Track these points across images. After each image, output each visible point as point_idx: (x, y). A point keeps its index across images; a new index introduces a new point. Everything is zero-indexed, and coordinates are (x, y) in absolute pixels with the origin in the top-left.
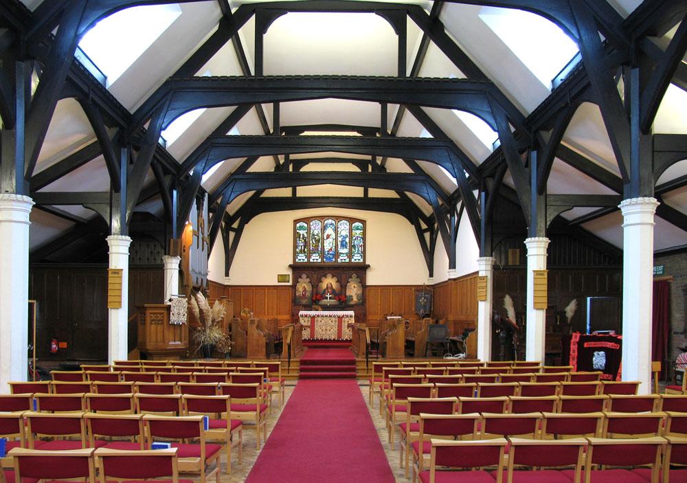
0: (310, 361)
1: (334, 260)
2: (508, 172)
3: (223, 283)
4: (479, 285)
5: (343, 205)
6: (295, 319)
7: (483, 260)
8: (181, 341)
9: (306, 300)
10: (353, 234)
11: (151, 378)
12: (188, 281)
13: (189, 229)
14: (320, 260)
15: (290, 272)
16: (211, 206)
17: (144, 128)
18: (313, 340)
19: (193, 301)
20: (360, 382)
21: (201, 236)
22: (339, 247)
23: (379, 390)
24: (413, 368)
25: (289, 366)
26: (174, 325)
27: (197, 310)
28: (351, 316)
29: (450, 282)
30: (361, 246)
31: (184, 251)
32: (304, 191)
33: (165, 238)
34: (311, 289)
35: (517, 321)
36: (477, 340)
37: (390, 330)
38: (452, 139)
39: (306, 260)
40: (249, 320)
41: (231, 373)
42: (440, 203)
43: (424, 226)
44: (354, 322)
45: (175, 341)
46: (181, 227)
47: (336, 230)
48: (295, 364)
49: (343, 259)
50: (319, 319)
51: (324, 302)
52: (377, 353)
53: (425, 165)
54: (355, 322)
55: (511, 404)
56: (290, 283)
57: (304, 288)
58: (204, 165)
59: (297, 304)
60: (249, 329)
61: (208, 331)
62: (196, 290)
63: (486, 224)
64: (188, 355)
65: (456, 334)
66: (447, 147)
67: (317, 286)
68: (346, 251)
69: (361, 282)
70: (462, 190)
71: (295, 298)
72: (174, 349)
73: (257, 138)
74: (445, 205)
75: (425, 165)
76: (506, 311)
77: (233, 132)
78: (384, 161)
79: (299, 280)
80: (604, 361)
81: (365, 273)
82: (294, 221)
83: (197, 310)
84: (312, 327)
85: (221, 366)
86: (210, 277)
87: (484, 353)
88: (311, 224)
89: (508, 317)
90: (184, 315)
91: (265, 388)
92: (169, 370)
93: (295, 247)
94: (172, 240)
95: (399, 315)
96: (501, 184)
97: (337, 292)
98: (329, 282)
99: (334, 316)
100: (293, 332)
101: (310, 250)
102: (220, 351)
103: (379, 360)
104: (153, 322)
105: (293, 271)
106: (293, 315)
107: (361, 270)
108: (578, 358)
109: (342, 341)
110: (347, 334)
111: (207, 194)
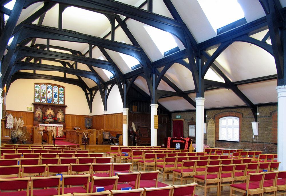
1: (51, 102)
5: (53, 79)
8: (9, 136)
9: (40, 119)
11: (45, 152)
14: (45, 102)
15: (33, 106)
24: (47, 150)
28: (62, 127)
34: (42, 114)
36: (123, 139)
43: (88, 92)
45: (7, 136)
47: (52, 90)
49: (55, 102)
50: (49, 127)
55: (49, 168)
56: (33, 111)
66: (113, 65)
67: (45, 113)
68: (56, 99)
69: (63, 113)
71: (35, 118)
72: (6, 140)
76: (133, 128)
79: (37, 110)
80: (179, 147)
81: (65, 109)
82: (34, 84)
85: (28, 149)
90: (12, 124)
92: (55, 149)
93: (35, 95)
95: (79, 127)
98: (50, 112)
99: (55, 127)
107: (63, 107)
108: (170, 145)
109: (58, 137)
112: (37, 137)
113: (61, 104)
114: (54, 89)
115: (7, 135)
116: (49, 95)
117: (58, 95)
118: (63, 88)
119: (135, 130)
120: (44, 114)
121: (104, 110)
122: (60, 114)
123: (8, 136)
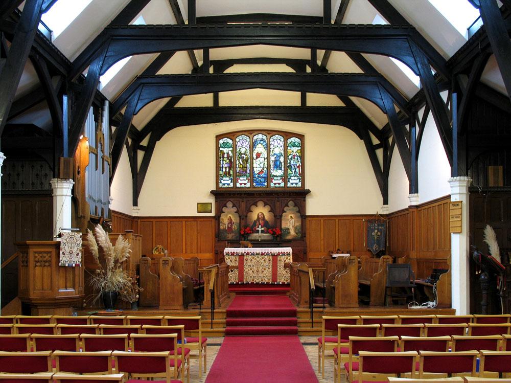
0: (240, 311)
1: (266, 184)
2: (492, 61)
3: (130, 215)
4: (453, 213)
5: (275, 116)
6: (219, 258)
7: (456, 181)
9: (233, 234)
10: (289, 151)
12: (84, 211)
13: (84, 146)
14: (248, 185)
15: (212, 200)
16: (113, 118)
17: (19, 11)
18: (243, 284)
19: (90, 236)
20: (303, 339)
21: (100, 154)
22: (272, 168)
23: (333, 354)
25: (212, 319)
26: (65, 267)
27: (95, 248)
28: (288, 254)
29: (411, 210)
30: (299, 167)
31: (79, 173)
32: (228, 99)
33: (54, 157)
35: (502, 259)
37: (339, 271)
38: (415, 26)
39: (232, 185)
40: (161, 260)
41: (132, 335)
42: (397, 110)
43: (376, 141)
44: (291, 261)
45: (66, 288)
46: (74, 143)
47: (268, 148)
48: (221, 316)
49: (277, 183)
50: (249, 257)
51: (255, 236)
52: (324, 302)
53: (375, 60)
54: (293, 261)
56: (213, 214)
57: (230, 219)
58: (101, 63)
59: (221, 239)
60: (162, 271)
61: (109, 274)
62: (94, 222)
63: (459, 134)
64: (85, 305)
65: (420, 276)
67: (246, 216)
68: (279, 173)
69: (299, 212)
70: (428, 91)
72: (65, 299)
73: (168, 27)
74: (403, 112)
75: (375, 60)
76: (487, 246)
77: (139, 21)
78: (326, 58)
79: (224, 209)
82: (217, 136)
83: (95, 248)
84: (240, 268)
86: (113, 207)
87: (460, 303)
88: (237, 140)
89: (490, 254)
91: (180, 353)
93: (218, 168)
94: (62, 159)
95: (348, 253)
96: (479, 85)
97: (270, 223)
98: (261, 211)
99: (268, 254)
100: (217, 274)
101: (236, 173)
102: (125, 300)
103: (326, 310)
104: (38, 264)
105: (216, 198)
106: (216, 253)
109: (278, 285)
110: (284, 276)
111: (107, 103)
112: (169, 288)
113: (294, 185)
114: (271, 146)
115: (68, 285)
116: (258, 163)
117: (286, 161)
118: (297, 140)
119: (494, 251)
120: (243, 221)
121: (410, 193)
122: (291, 217)
123: (72, 290)
